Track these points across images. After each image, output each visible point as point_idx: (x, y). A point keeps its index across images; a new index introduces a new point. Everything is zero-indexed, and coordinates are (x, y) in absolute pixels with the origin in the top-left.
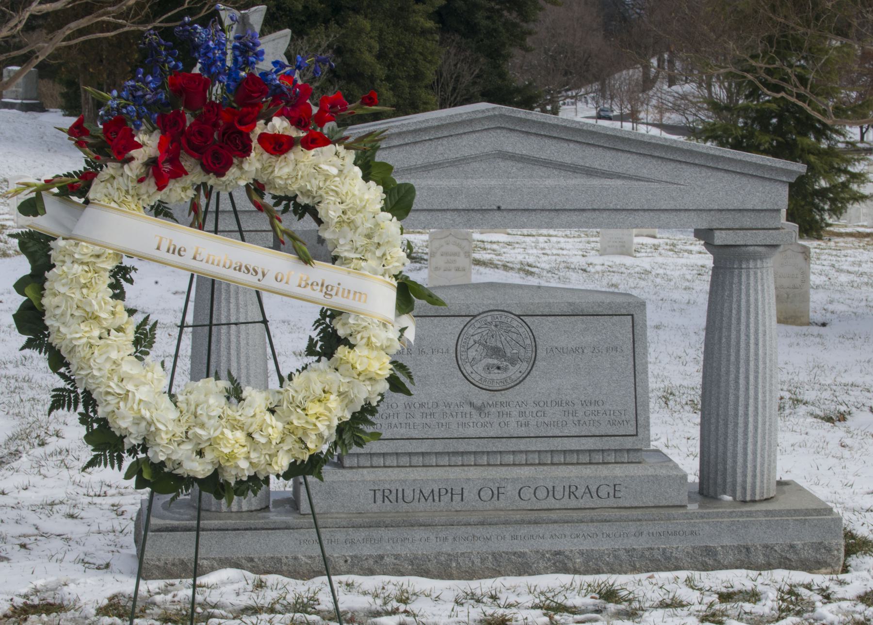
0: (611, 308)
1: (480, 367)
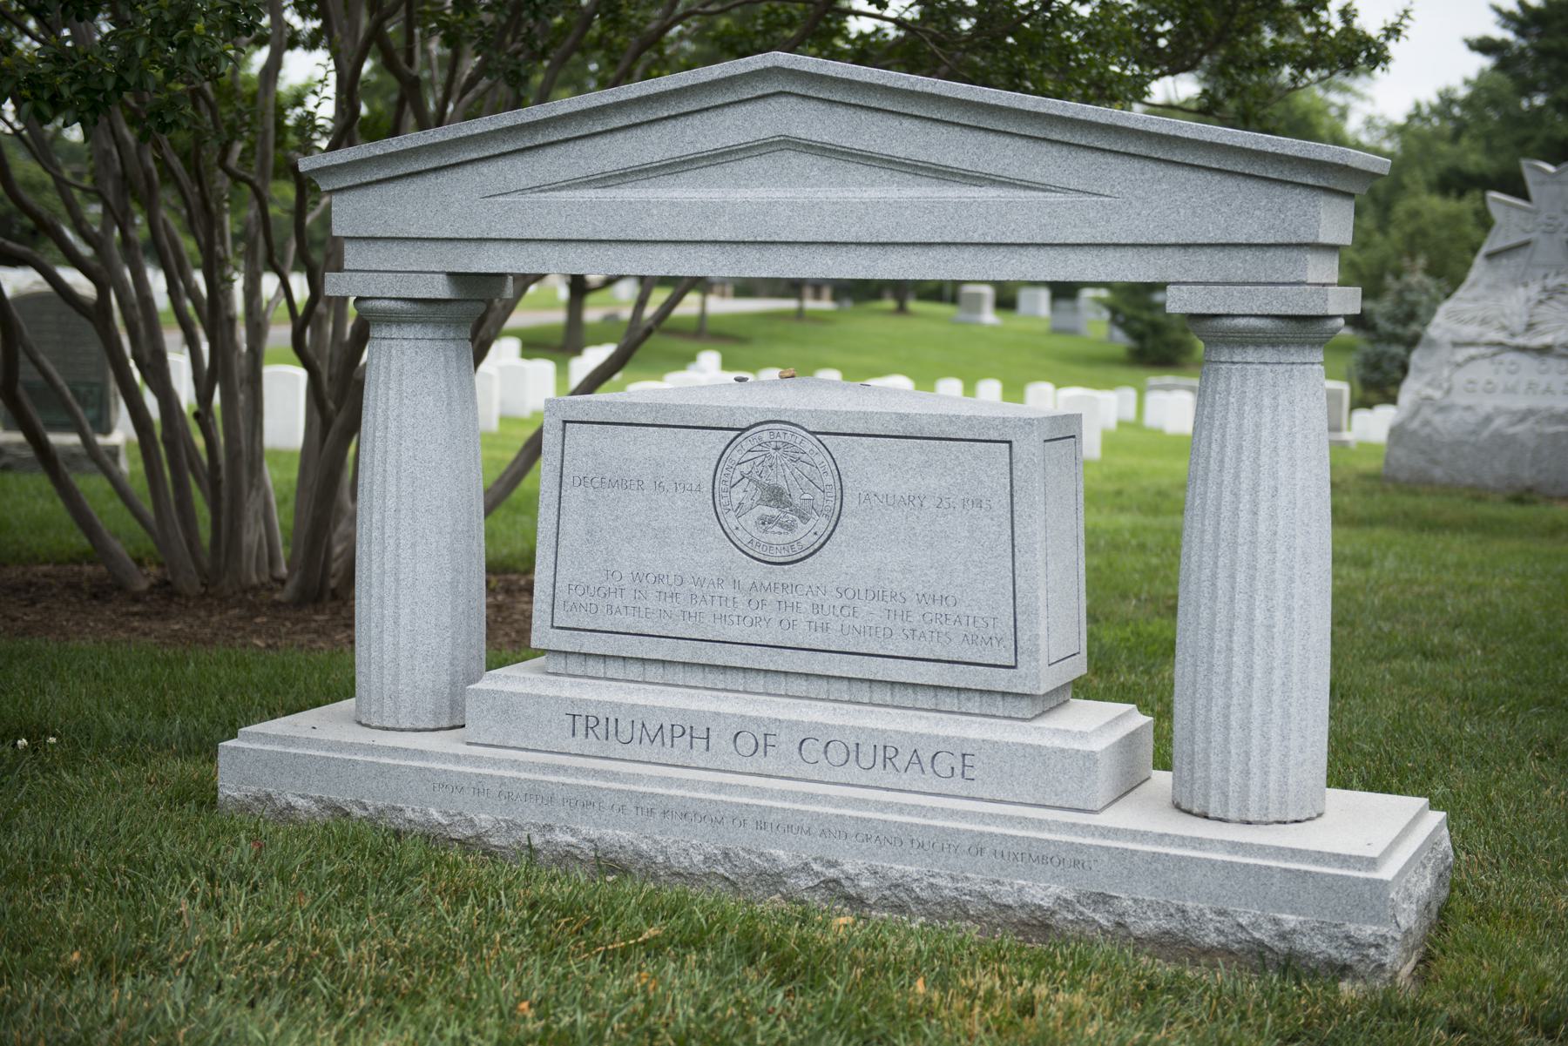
0: (971, 427)
1: (750, 520)
